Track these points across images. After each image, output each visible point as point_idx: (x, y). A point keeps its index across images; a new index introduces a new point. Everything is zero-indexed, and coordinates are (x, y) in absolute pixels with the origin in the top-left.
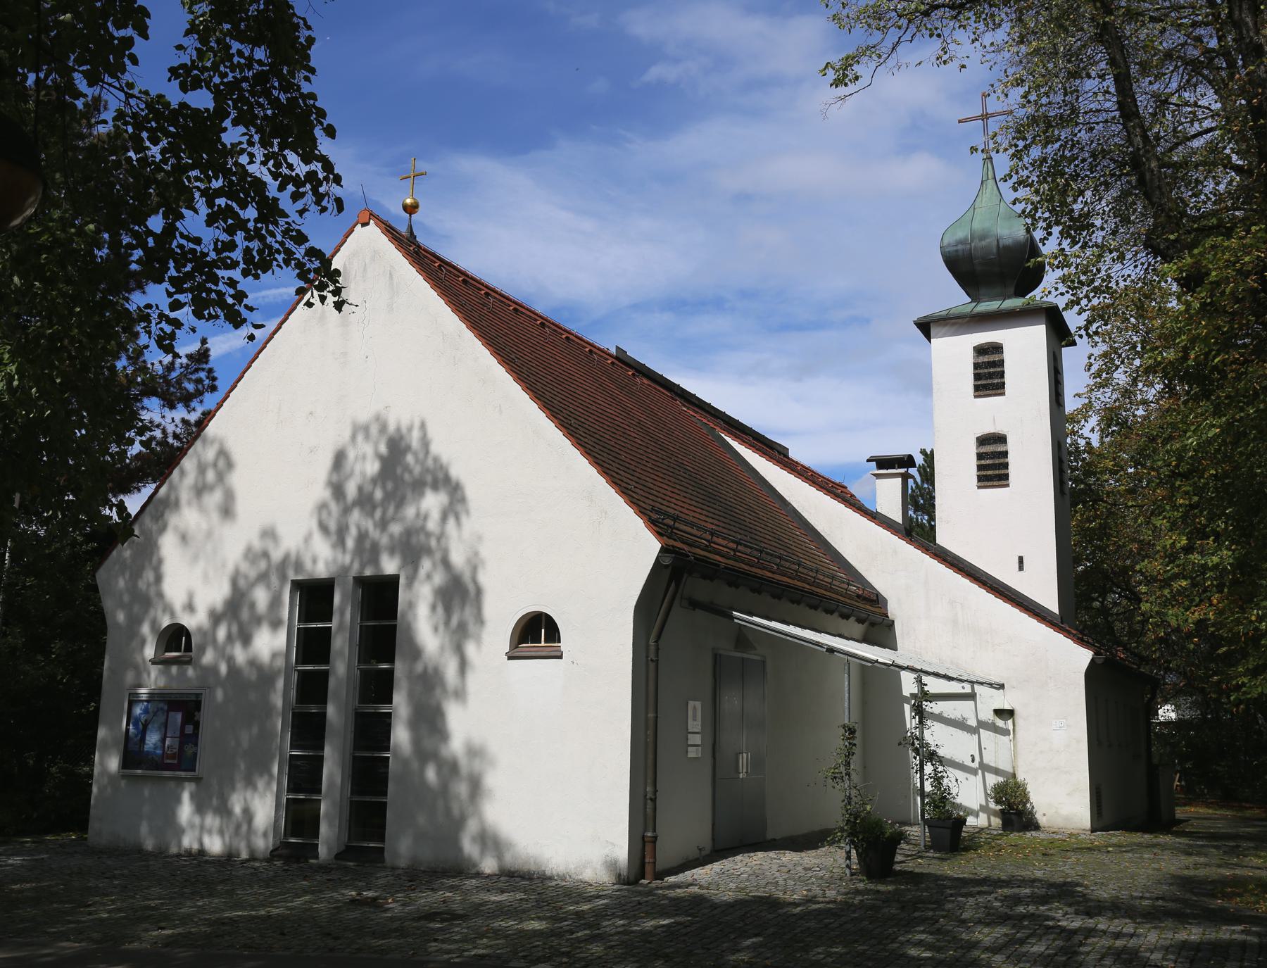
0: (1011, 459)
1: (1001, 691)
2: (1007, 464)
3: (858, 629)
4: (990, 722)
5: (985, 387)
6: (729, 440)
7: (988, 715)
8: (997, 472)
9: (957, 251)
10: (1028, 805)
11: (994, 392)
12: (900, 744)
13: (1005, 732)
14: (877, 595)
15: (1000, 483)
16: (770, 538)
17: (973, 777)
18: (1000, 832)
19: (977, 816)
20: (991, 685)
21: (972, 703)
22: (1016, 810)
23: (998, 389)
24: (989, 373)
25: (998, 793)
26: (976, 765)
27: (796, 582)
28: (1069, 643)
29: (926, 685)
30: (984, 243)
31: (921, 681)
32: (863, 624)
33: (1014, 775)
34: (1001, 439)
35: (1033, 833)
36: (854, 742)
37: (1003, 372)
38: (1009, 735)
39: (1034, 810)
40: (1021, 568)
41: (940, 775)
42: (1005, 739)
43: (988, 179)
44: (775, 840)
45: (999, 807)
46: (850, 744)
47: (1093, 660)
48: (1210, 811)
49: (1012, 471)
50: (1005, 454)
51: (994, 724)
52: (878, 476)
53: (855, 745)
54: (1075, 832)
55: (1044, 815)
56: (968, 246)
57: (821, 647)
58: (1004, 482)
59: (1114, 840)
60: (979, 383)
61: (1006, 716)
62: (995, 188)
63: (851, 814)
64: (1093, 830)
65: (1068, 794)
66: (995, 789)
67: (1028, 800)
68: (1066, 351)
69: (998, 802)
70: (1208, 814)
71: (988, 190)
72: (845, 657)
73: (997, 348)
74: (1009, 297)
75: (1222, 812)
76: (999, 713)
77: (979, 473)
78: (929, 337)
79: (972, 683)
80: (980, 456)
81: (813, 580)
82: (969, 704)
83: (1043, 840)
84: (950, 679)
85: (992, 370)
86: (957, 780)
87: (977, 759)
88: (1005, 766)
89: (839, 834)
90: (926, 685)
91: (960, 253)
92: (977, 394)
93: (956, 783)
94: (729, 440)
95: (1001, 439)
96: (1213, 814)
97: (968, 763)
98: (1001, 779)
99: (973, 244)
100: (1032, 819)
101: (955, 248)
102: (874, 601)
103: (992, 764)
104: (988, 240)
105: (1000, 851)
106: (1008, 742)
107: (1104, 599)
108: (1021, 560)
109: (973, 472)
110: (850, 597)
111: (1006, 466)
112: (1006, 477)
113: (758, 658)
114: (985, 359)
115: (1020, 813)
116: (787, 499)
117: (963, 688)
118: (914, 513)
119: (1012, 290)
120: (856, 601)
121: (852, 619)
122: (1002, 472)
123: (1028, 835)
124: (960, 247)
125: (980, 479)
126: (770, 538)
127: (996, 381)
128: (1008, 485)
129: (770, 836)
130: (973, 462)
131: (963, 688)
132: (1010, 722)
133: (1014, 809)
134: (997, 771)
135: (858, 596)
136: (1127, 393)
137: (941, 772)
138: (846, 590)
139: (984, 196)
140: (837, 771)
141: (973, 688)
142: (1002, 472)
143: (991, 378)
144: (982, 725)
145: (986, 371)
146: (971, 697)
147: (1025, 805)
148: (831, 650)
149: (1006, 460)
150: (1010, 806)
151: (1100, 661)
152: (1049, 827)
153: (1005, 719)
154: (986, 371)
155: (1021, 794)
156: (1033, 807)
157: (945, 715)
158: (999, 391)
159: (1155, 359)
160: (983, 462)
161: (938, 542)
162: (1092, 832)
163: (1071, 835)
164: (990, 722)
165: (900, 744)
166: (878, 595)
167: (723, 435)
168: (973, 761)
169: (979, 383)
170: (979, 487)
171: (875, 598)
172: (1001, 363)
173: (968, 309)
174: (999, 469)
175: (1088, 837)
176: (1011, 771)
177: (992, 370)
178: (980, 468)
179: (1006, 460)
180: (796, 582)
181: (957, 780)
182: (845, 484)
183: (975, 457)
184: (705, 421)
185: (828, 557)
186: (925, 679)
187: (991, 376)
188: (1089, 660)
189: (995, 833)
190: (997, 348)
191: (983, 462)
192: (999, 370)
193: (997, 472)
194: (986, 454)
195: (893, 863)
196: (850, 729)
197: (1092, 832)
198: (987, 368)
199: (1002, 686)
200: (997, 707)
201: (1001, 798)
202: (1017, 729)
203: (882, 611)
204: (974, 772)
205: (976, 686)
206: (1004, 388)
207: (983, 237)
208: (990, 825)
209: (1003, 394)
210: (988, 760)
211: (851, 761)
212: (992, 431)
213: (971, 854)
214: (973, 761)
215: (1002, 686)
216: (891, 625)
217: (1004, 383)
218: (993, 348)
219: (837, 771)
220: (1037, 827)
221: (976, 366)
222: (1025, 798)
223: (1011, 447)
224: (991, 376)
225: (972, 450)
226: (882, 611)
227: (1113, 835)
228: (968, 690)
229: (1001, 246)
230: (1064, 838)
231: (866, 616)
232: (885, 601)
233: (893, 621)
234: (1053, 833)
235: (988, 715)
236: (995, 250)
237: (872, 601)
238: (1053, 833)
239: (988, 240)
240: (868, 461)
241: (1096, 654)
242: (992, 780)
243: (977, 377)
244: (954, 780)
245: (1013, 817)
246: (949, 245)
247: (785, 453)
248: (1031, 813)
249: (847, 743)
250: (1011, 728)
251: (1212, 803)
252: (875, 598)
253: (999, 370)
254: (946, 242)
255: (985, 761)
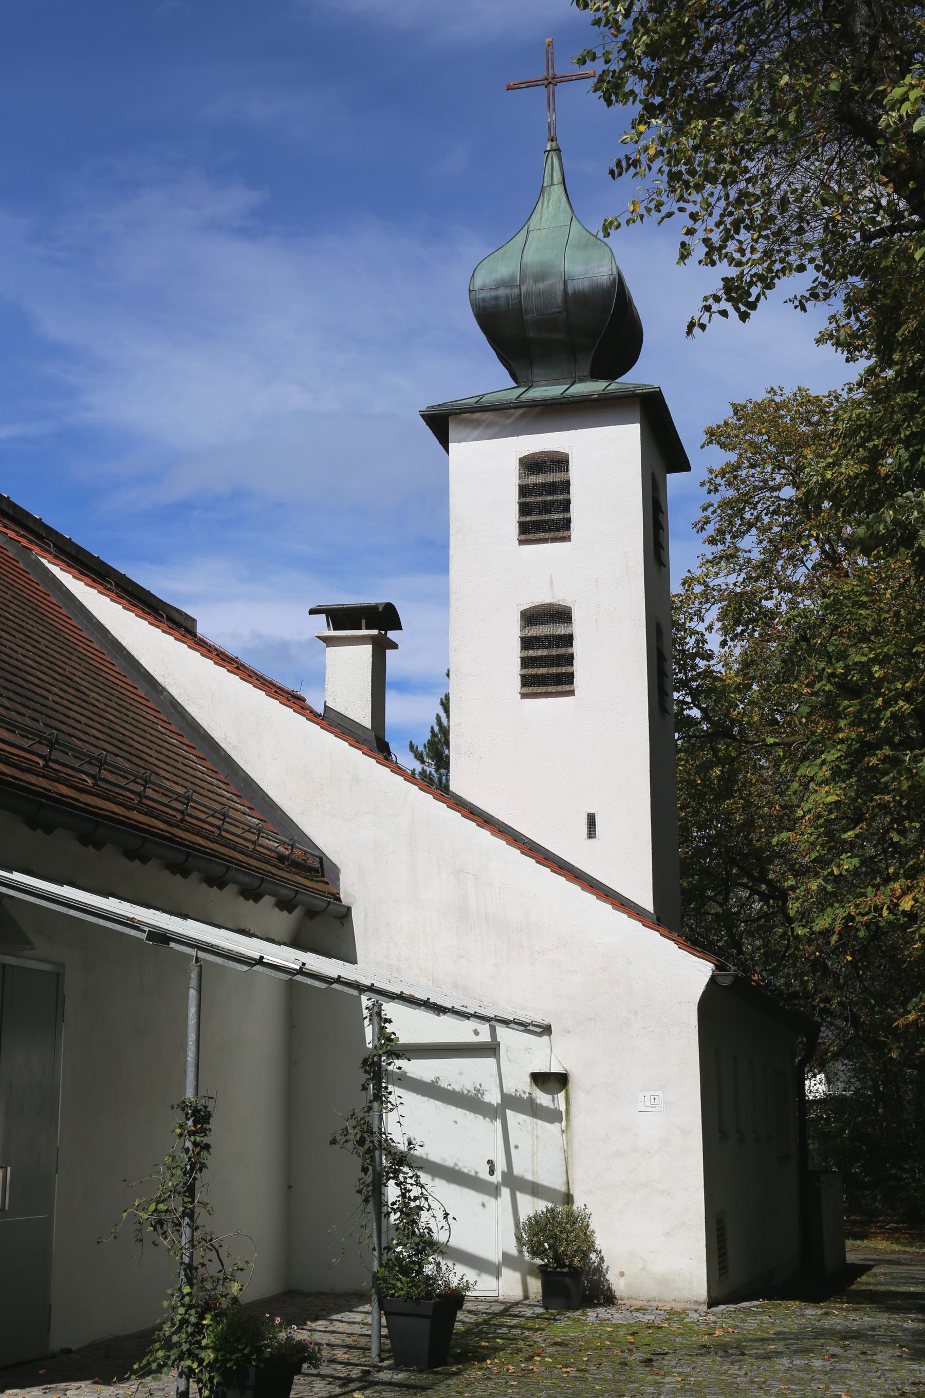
0: (578, 648)
1: (546, 1038)
2: (572, 656)
3: (283, 921)
4: (526, 1096)
5: (538, 527)
6: (55, 570)
7: (521, 1084)
8: (554, 670)
9: (497, 298)
10: (593, 1256)
11: (551, 535)
12: (334, 1142)
13: (552, 1116)
14: (321, 859)
15: (560, 688)
16: (99, 735)
17: (493, 1200)
18: (540, 1310)
19: (498, 1275)
20: (524, 1026)
21: (492, 1061)
22: (570, 1266)
23: (558, 530)
24: (545, 502)
25: (536, 1234)
26: (497, 1178)
27: (135, 815)
28: (670, 946)
29: (390, 1021)
30: (541, 286)
31: (379, 1014)
32: (290, 912)
33: (568, 1198)
34: (562, 615)
35: (601, 1311)
36: (206, 1140)
37: (568, 502)
38: (560, 1121)
39: (605, 1266)
40: (592, 831)
41: (413, 1204)
42: (554, 1129)
43: (552, 184)
44: (68, 1351)
45: (538, 1261)
46: (195, 1144)
47: (713, 980)
48: (896, 1247)
49: (580, 668)
50: (568, 640)
51: (531, 1100)
52: (329, 641)
53: (207, 1147)
54: (678, 1307)
55: (622, 1274)
56: (516, 291)
57: (137, 928)
58: (566, 688)
59: (751, 1324)
60: (528, 519)
61: (553, 1084)
62: (564, 198)
63: (190, 1307)
64: (712, 1303)
65: (667, 1234)
66: (531, 1224)
67: (591, 1247)
68: (673, 480)
69: (534, 1253)
70: (893, 1252)
71: (552, 203)
72: (192, 952)
73: (559, 462)
74: (582, 380)
75: (914, 1249)
76: (541, 1079)
77: (525, 672)
78: (445, 442)
79: (493, 1021)
80: (527, 643)
81: (179, 816)
82: (489, 1063)
83: (617, 1326)
84: (439, 1009)
85: (549, 498)
86: (446, 1215)
87: (501, 1166)
88: (556, 1182)
89: (160, 1354)
90: (390, 1021)
91: (502, 302)
92: (523, 537)
93: (444, 1223)
94: (55, 570)
95: (562, 615)
96: (899, 1252)
97: (484, 1174)
98: (542, 1206)
99: (524, 288)
100: (599, 1282)
101: (494, 293)
102: (316, 871)
103: (529, 1177)
104: (547, 282)
105: (530, 1359)
106: (559, 1135)
107: (726, 899)
108: (591, 820)
109: (514, 670)
110: (261, 858)
111: (569, 660)
112: (569, 678)
113: (47, 967)
114: (540, 479)
115: (576, 1273)
116: (160, 679)
117: (476, 1033)
118: (437, 771)
119: (586, 372)
120: (275, 866)
121: (268, 900)
122: (563, 670)
123: (591, 1314)
124: (502, 292)
125: (526, 681)
126: (99, 735)
127: (555, 516)
128: (571, 693)
129: (57, 1343)
130: (514, 653)
131: (476, 1033)
132: (561, 1096)
133: (564, 1266)
134: (535, 1190)
135: (281, 858)
136: (765, 569)
137: (416, 1199)
138: (254, 843)
139: (545, 210)
140: (162, 1207)
141: (493, 1030)
142: (563, 670)
143: (549, 512)
144: (511, 1102)
145: (539, 499)
146: (490, 1049)
147: (585, 1255)
148: (161, 937)
149: (570, 650)
150: (558, 1258)
151: (725, 981)
152: (630, 1298)
153: (553, 1092)
154: (539, 499)
155: (577, 1236)
156: (602, 1259)
157: (443, 1084)
158: (561, 534)
159: (823, 476)
160: (531, 653)
161: (452, 788)
162: (709, 1307)
163: (672, 1312)
164: (526, 1096)
165: (334, 1142)
166: (322, 859)
167: (45, 561)
168: (492, 1172)
169: (528, 519)
170: (524, 696)
171: (317, 865)
172: (565, 486)
173: (513, 395)
174: (558, 646)
175: (700, 1316)
176: (563, 1189)
177: (549, 498)
178: (526, 662)
179: (570, 650)
180: (135, 815)
181: (446, 1215)
182: (302, 694)
183: (517, 644)
184: (12, 534)
185: (232, 788)
186: (390, 1009)
187: (547, 508)
188: (706, 980)
189: (528, 1312)
190: (559, 462)
191: (531, 653)
192: (561, 497)
193: (554, 670)
194: (537, 638)
195: (818, 1037)
196: (196, 1111)
197: (709, 1307)
198: (541, 495)
199: (546, 1030)
200: (537, 1070)
201: (541, 1244)
202: (574, 1109)
203: (330, 888)
204: (495, 1191)
205: (501, 1030)
206: (568, 528)
207: (541, 276)
208: (526, 1297)
209: (567, 539)
210: (519, 1170)
211: (198, 1184)
212: (548, 600)
213: (474, 1373)
214: (492, 1172)
215: (546, 1030)
216: (345, 915)
217: (569, 521)
218: (553, 462)
219: (162, 1207)
220: (609, 1299)
221: (524, 491)
222: (586, 1244)
223: (579, 628)
224: (547, 508)
225: (513, 632)
226: (330, 888)
227: (748, 1312)
228: (485, 1036)
229: (570, 292)
230: (658, 1321)
231: (292, 894)
232: (336, 870)
233: (349, 909)
234: (638, 1310)
235: (521, 1084)
236: (559, 299)
237: (311, 869)
238: (638, 1310)
239: (547, 282)
240: (312, 612)
241: (719, 967)
242: (530, 1207)
243: (524, 509)
244: (440, 1215)
245: (568, 1281)
246: (483, 288)
247: (189, 625)
248: (599, 1271)
249: (189, 1144)
250: (563, 1108)
251: (894, 1230)
252: (317, 865)
253: (561, 497)
254: (478, 283)
255: (517, 1171)
